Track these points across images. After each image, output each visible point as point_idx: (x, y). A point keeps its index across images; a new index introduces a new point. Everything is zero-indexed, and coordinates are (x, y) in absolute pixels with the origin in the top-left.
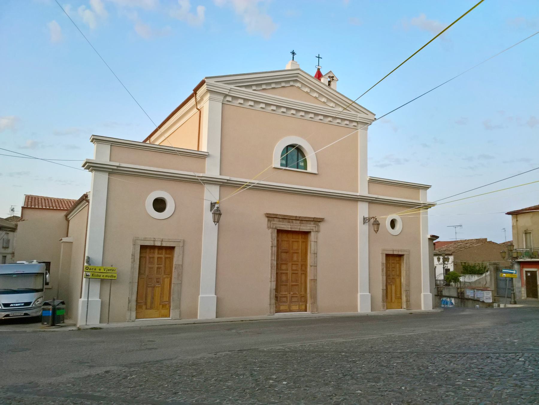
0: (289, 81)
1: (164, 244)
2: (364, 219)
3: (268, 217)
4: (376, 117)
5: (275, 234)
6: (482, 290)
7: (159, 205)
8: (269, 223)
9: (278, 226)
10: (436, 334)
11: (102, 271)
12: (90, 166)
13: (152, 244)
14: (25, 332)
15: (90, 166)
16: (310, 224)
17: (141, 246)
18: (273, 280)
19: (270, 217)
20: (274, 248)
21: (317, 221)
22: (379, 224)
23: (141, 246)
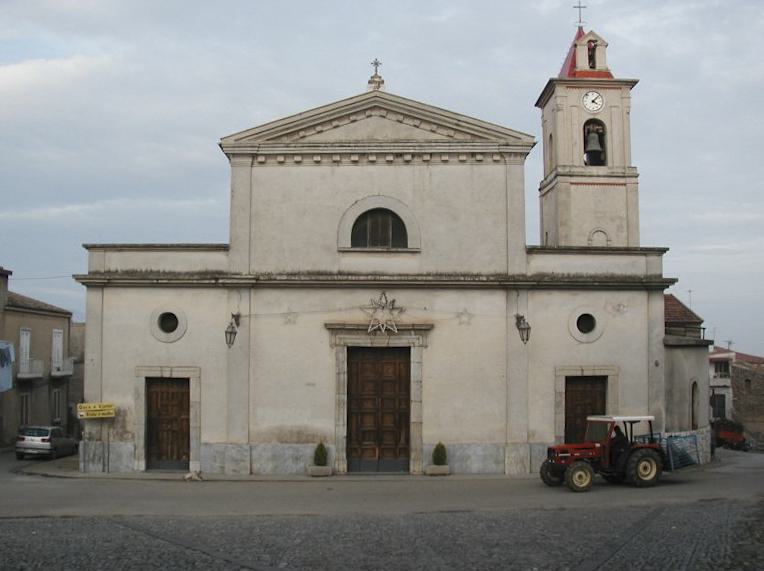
0: (331, 121)
1: (175, 375)
2: (286, 323)
3: (329, 329)
4: (535, 140)
5: (344, 356)
6: (732, 447)
7: (586, 323)
8: (333, 337)
9: (348, 341)
10: (215, 532)
11: (98, 408)
12: (673, 281)
13: (159, 375)
14: (717, 473)
15: (673, 281)
16: (411, 334)
17: (147, 379)
18: (341, 423)
19: (334, 329)
20: (342, 376)
21: (424, 329)
22: (529, 328)
23: (147, 379)
